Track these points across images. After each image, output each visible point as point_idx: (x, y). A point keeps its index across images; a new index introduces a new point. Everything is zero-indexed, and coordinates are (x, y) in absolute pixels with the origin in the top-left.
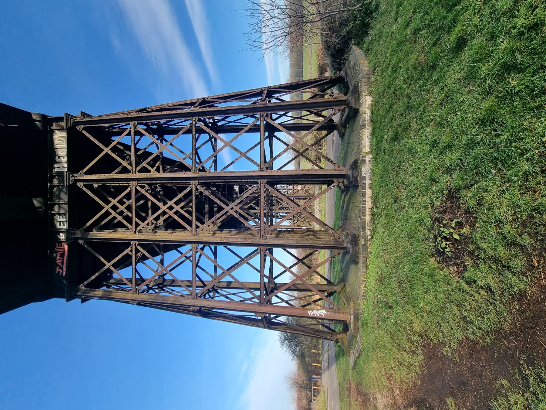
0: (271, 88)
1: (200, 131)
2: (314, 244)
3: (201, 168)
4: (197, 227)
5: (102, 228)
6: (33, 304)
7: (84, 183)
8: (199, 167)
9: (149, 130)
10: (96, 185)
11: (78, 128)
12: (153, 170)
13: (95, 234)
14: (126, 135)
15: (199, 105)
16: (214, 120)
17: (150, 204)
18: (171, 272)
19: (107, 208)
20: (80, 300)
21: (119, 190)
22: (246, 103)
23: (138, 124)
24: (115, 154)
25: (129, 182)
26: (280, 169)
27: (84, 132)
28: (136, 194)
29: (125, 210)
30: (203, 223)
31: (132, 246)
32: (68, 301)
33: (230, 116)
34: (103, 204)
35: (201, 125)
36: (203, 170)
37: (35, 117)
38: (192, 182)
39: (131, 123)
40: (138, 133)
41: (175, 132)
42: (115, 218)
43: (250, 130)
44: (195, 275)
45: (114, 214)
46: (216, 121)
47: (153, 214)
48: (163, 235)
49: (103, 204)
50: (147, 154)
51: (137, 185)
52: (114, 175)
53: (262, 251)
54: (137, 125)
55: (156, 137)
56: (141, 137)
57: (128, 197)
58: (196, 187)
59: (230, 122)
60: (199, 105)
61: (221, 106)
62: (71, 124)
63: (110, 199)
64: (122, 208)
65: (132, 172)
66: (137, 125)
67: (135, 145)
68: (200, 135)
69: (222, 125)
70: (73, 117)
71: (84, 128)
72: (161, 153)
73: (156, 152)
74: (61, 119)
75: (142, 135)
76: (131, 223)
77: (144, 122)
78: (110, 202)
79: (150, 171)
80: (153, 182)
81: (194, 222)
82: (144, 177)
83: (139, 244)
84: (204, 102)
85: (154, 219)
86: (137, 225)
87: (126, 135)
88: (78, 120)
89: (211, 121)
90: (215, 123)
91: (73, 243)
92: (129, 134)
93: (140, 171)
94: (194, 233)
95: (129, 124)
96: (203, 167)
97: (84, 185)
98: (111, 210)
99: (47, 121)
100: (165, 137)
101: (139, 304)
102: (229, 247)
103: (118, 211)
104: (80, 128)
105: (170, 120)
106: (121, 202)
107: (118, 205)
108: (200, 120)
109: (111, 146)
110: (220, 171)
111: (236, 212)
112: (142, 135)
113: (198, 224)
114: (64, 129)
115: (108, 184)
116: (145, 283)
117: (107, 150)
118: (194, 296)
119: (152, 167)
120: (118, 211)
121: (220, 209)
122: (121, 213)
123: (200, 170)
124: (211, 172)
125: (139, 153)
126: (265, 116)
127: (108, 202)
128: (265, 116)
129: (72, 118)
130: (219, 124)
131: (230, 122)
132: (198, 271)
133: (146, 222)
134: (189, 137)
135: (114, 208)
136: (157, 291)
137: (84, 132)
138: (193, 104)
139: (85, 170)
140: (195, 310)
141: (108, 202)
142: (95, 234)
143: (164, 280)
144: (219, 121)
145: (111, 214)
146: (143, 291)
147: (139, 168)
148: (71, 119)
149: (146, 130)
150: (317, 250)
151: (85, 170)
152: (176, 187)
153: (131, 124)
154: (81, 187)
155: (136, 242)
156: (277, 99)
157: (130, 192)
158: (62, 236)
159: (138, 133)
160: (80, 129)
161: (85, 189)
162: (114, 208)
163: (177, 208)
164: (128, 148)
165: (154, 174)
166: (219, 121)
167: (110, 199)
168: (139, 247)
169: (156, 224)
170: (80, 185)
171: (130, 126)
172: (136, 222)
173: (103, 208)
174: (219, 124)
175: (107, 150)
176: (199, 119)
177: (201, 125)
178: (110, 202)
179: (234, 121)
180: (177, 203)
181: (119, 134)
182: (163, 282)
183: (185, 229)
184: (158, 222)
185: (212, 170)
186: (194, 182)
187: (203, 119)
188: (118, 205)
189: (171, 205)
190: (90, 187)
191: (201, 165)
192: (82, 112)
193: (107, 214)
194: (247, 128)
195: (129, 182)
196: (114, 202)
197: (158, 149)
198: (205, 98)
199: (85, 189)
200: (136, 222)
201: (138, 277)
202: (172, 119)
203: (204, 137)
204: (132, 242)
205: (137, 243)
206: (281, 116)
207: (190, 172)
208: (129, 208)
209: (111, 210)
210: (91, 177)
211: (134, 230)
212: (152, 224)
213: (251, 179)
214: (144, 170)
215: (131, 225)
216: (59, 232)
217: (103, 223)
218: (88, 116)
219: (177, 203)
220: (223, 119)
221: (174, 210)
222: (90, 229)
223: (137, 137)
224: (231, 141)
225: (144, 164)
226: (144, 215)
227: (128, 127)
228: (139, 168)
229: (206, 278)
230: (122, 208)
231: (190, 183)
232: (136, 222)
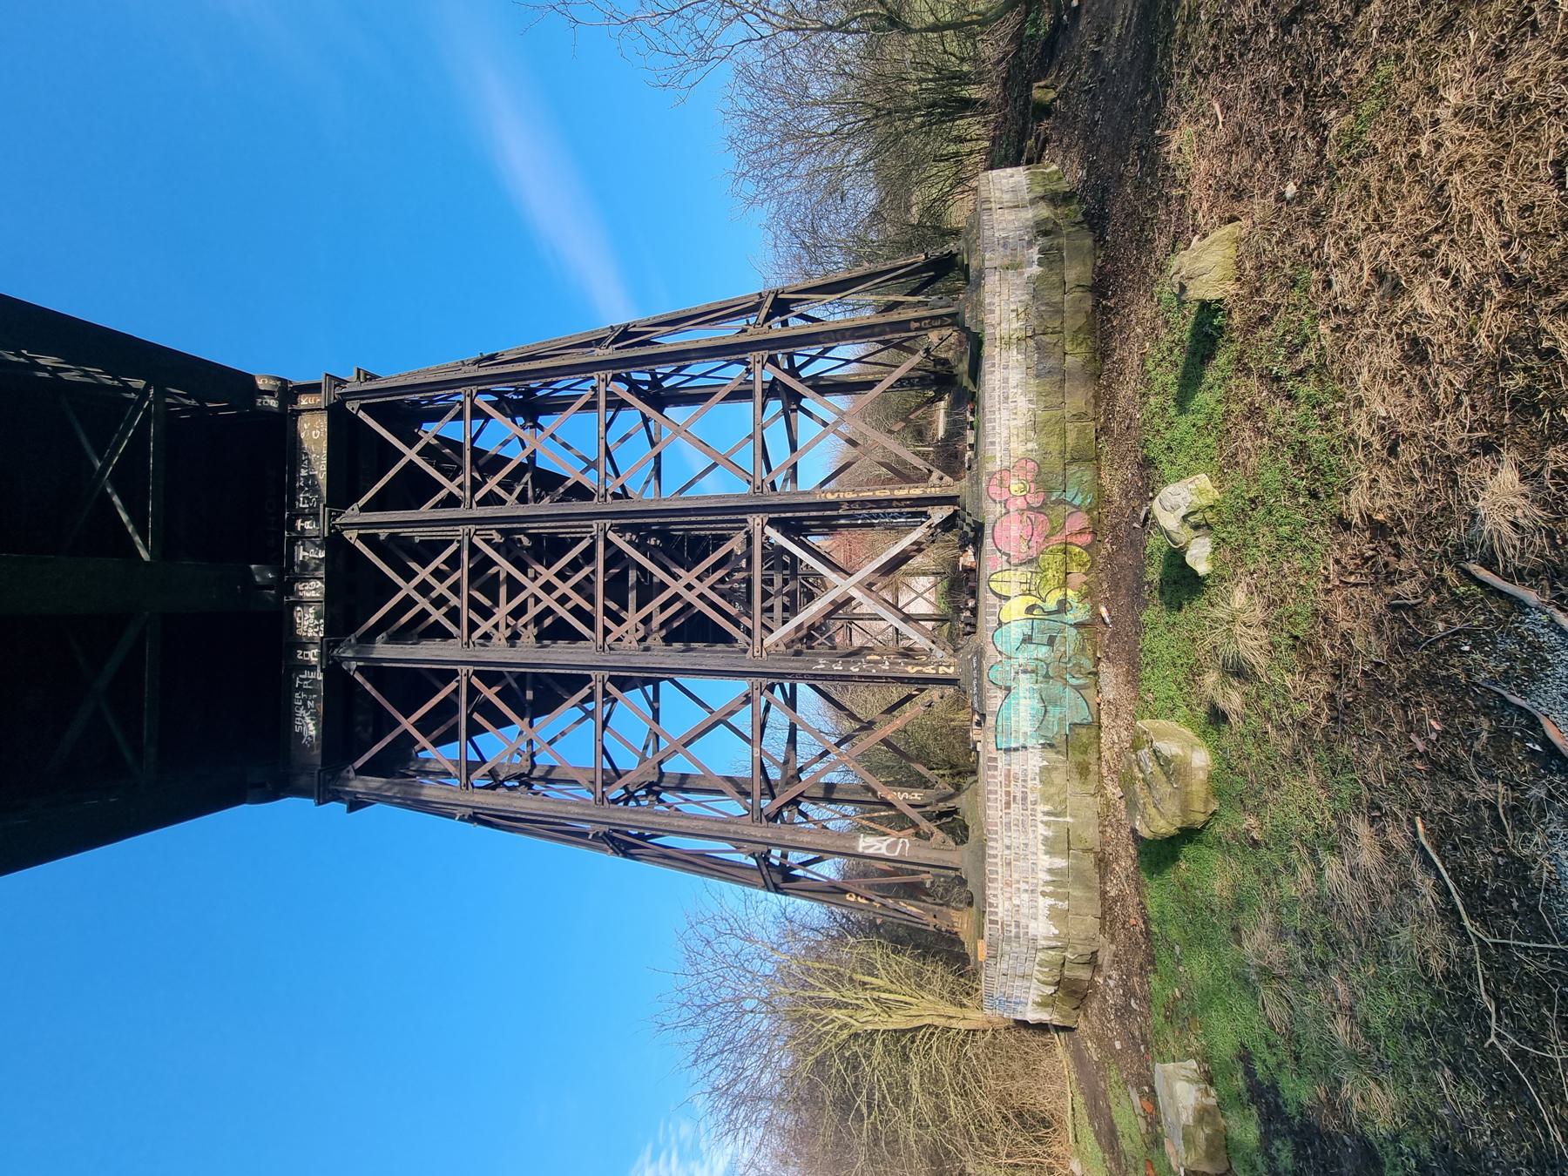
0: (783, 293)
1: (617, 404)
4: (607, 631)
5: (399, 637)
6: (244, 809)
7: (771, 516)
9: (501, 404)
10: (383, 534)
11: (349, 406)
12: (511, 499)
13: (385, 651)
15: (613, 342)
16: (653, 375)
17: (633, 576)
18: (552, 746)
19: (407, 588)
21: (436, 547)
22: (727, 332)
23: (479, 392)
24: (431, 465)
25: (740, 517)
27: (361, 414)
30: (619, 621)
31: (458, 678)
32: (319, 804)
34: (400, 581)
35: (621, 389)
36: (623, 494)
37: (262, 384)
39: (595, 374)
40: (477, 413)
41: (561, 406)
42: (424, 614)
43: (734, 396)
44: (600, 749)
45: (423, 603)
46: (659, 376)
47: (509, 600)
48: (529, 653)
49: (400, 581)
50: (499, 462)
51: (475, 534)
52: (425, 512)
55: (520, 420)
56: (487, 421)
58: (470, 540)
59: (693, 377)
60: (613, 342)
61: (671, 341)
63: (414, 566)
64: (441, 589)
65: (596, 497)
67: (473, 440)
69: (673, 387)
70: (341, 382)
71: (362, 407)
72: (532, 458)
73: (518, 456)
74: (314, 388)
75: (488, 418)
76: (457, 623)
78: (415, 574)
80: (515, 526)
81: (601, 620)
83: (476, 673)
84: (625, 335)
85: (510, 614)
86: (473, 626)
88: (349, 388)
90: (656, 382)
91: (334, 671)
92: (459, 416)
95: (592, 378)
97: (360, 537)
98: (416, 596)
99: (289, 393)
100: (542, 420)
101: (474, 818)
103: (434, 595)
104: (352, 406)
107: (433, 581)
108: (616, 378)
110: (668, 495)
111: (701, 596)
112: (488, 418)
113: (610, 625)
114: (321, 409)
115: (405, 532)
117: (411, 454)
120: (434, 595)
121: (648, 589)
122: (440, 602)
124: (644, 496)
126: (609, 379)
127: (408, 575)
128: (609, 379)
129: (339, 385)
130: (666, 384)
131: (693, 377)
133: (492, 621)
134: (593, 420)
135: (424, 588)
136: (644, 802)
137: (361, 414)
139: (362, 502)
140: (600, 835)
141: (408, 575)
142: (385, 651)
143: (662, 774)
144: (666, 376)
146: (615, 801)
147: (479, 495)
148: (335, 386)
149: (495, 405)
150: (925, 689)
151: (362, 502)
152: (529, 536)
153: (596, 377)
154: (352, 542)
155: (468, 667)
156: (801, 316)
157: (458, 553)
158: (313, 655)
159: (477, 413)
162: (424, 588)
164: (457, 447)
165: (512, 507)
166: (666, 376)
167: (414, 566)
170: (351, 535)
171: (594, 383)
172: (470, 620)
174: (666, 384)
175: (411, 454)
176: (613, 375)
177: (621, 389)
178: (415, 574)
179: (704, 375)
180: (562, 576)
181: (437, 416)
182: (660, 780)
183: (581, 637)
184: (520, 621)
185: (651, 492)
186: (466, 528)
188: (433, 581)
190: (369, 540)
191: (620, 482)
193: (408, 603)
196: (424, 574)
197: (524, 446)
200: (470, 620)
201: (607, 766)
203: (629, 420)
204: (459, 668)
206: (812, 359)
209: (416, 596)
210: (443, 514)
211: (465, 639)
212: (508, 626)
213: (736, 512)
214: (491, 499)
215: (459, 628)
216: (304, 645)
217: (404, 619)
218: (373, 377)
220: (677, 371)
221: (556, 594)
224: (688, 423)
225: (492, 484)
226: (487, 602)
227: (587, 385)
228: (479, 495)
229: (626, 760)
230: (441, 589)
231: (745, 521)
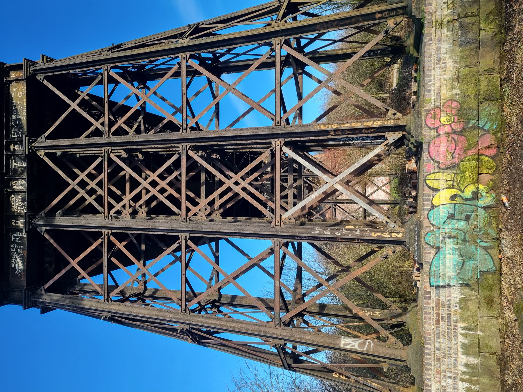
2: (241, 230)
3: (195, 126)
4: (188, 210)
8: (191, 123)
9: (125, 74)
10: (59, 152)
11: (38, 77)
12: (132, 131)
14: (97, 84)
16: (214, 54)
17: (203, 176)
19: (73, 184)
20: (39, 310)
21: (88, 160)
23: (112, 68)
24: (85, 111)
25: (267, 141)
26: (232, 125)
27: (45, 82)
28: (187, 161)
29: (96, 188)
31: (103, 237)
32: (25, 309)
33: (326, 33)
35: (195, 64)
36: (197, 128)
38: (181, 146)
42: (83, 199)
45: (82, 193)
46: (218, 55)
47: (131, 192)
50: (125, 109)
52: (82, 139)
53: (278, 245)
54: (110, 69)
55: (136, 84)
56: (117, 85)
57: (99, 169)
58: (109, 156)
59: (238, 55)
60: (190, 35)
62: (30, 73)
63: (77, 171)
64: (92, 184)
65: (181, 129)
66: (110, 69)
67: (109, 96)
68: (193, 76)
69: (226, 62)
70: (34, 63)
74: (18, 68)
77: (120, 64)
79: (127, 133)
80: (134, 147)
81: (184, 203)
82: (60, 144)
84: (197, 30)
87: (97, 84)
88: (38, 67)
89: (211, 56)
92: (101, 82)
93: (115, 134)
94: (106, 216)
96: (197, 123)
97: (46, 154)
98: (78, 189)
100: (149, 83)
101: (112, 319)
102: (230, 238)
103: (88, 188)
104: (40, 77)
105: (152, 59)
106: (91, 176)
108: (192, 57)
109: (78, 101)
111: (244, 189)
112: (117, 83)
115: (71, 151)
116: (196, 300)
118: (183, 309)
119: (131, 127)
120: (88, 188)
122: (91, 192)
123: (192, 129)
125: (114, 109)
126: (188, 58)
127: (74, 176)
128: (188, 58)
129: (32, 65)
130: (222, 60)
131: (238, 55)
132: (190, 275)
133: (122, 203)
135: (83, 184)
137: (45, 82)
138: (181, 35)
139: (46, 134)
140: (184, 330)
141: (74, 176)
144: (222, 55)
145: (78, 193)
149: (121, 75)
151: (46, 134)
153: (180, 57)
158: (21, 223)
159: (111, 80)
160: (40, 79)
161: (46, 159)
162: (83, 184)
163: (244, 184)
164: (100, 100)
165: (132, 136)
167: (77, 171)
168: (112, 238)
169: (135, 206)
170: (41, 153)
171: (179, 60)
172: (109, 202)
173: (69, 185)
174: (222, 60)
175: (74, 105)
179: (245, 53)
180: (162, 177)
181: (88, 82)
187: (197, 55)
189: (154, 180)
190: (51, 156)
192: (25, 59)
193: (74, 192)
194: (257, 64)
195: (267, 141)
196: (82, 176)
198: (199, 24)
199: (46, 159)
200: (109, 202)
201: (188, 290)
202: (156, 59)
205: (110, 231)
206: (312, 41)
207: (179, 131)
208: (100, 184)
209: (78, 189)
211: (106, 214)
212: (130, 206)
214: (120, 132)
216: (16, 217)
219: (162, 177)
221: (158, 188)
222: (52, 213)
223: (112, 86)
224: (235, 83)
225: (120, 123)
226: (119, 193)
227: (175, 62)
230: (92, 184)
231: (270, 143)
232: (109, 203)
